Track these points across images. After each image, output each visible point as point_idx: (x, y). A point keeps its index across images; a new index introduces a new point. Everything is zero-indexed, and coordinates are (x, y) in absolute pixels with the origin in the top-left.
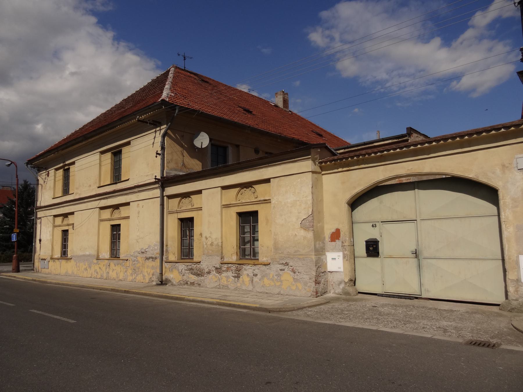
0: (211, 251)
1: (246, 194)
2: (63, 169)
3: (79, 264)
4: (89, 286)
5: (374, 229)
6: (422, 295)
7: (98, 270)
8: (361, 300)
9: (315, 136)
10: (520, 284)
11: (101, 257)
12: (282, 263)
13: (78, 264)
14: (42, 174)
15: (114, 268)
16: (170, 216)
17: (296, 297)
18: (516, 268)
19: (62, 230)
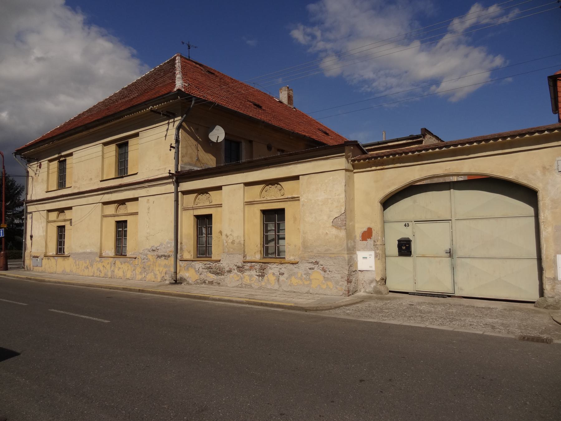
0: (232, 250)
1: (272, 191)
2: (58, 161)
3: (79, 262)
4: (96, 285)
5: (407, 228)
6: (455, 293)
7: (102, 268)
8: (394, 298)
9: (322, 134)
10: (556, 282)
11: (104, 254)
12: (311, 261)
13: (77, 263)
14: (32, 165)
15: (120, 266)
16: (184, 213)
17: (327, 296)
18: (553, 267)
19: (57, 226)
